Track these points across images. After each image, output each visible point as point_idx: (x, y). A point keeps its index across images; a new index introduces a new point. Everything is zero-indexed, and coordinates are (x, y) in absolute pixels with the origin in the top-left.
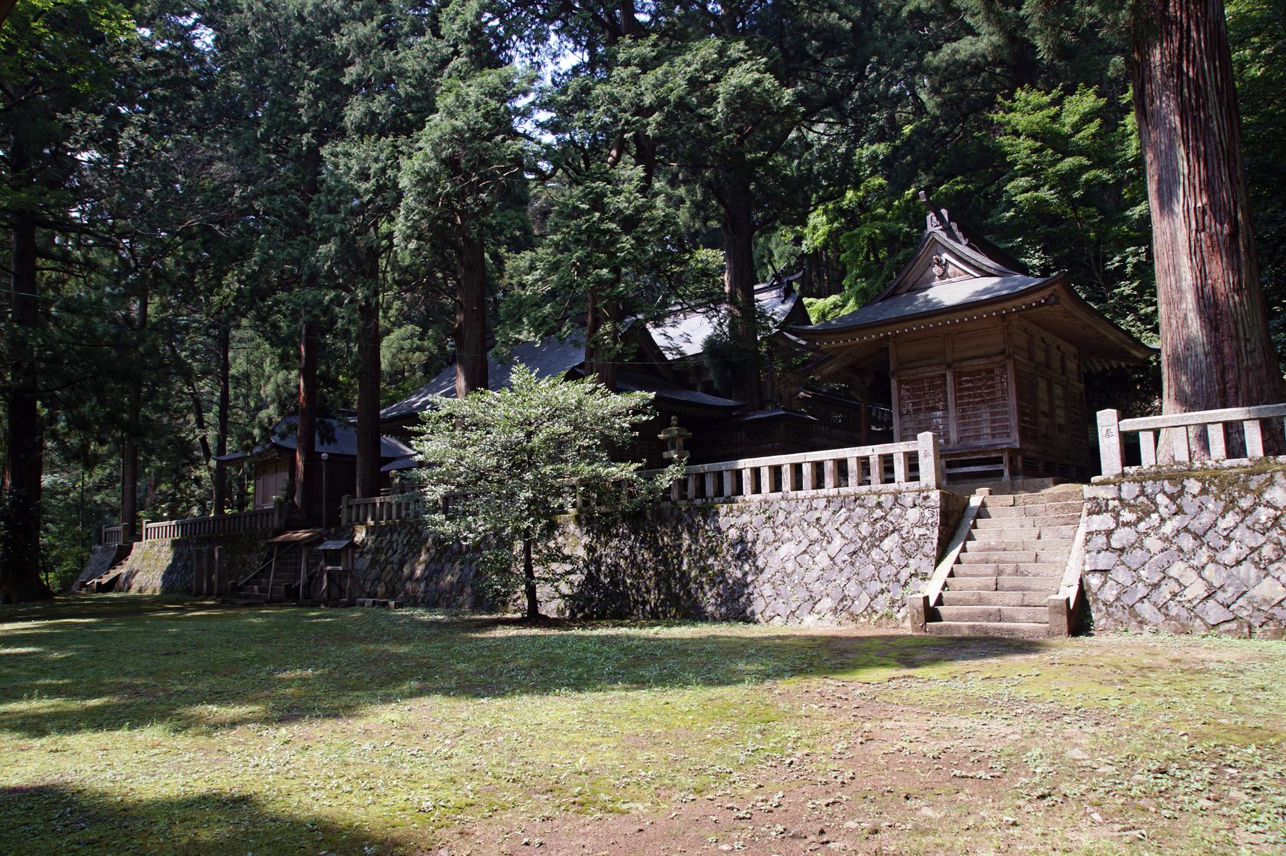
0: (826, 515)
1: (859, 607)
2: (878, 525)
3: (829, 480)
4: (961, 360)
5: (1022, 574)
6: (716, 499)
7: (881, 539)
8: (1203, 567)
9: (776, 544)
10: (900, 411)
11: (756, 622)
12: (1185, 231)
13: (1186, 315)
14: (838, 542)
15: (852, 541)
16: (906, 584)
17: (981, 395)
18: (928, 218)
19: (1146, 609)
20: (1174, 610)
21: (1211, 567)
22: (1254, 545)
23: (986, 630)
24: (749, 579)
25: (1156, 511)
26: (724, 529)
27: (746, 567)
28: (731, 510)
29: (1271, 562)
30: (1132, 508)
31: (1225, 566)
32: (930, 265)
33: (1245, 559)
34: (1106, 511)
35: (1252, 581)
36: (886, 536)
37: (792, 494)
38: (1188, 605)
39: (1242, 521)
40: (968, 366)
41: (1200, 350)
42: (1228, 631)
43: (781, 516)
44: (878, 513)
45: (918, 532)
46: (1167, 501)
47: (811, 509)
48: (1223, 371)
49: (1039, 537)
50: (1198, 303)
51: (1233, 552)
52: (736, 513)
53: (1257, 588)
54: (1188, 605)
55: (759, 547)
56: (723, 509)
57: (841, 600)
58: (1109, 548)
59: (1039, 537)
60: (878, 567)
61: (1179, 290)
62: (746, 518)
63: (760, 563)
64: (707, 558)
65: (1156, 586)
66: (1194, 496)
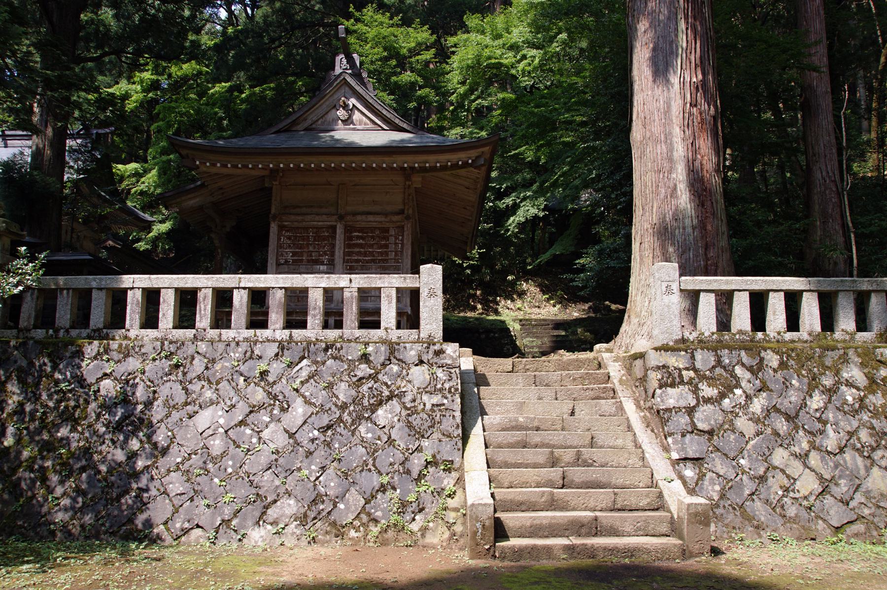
0: (276, 368)
1: (347, 511)
2: (365, 388)
3: (276, 317)
4: (355, 214)
5: (586, 464)
6: (74, 333)
7: (374, 408)
8: (807, 455)
9: (190, 408)
10: (277, 260)
11: (155, 540)
12: (680, 102)
13: (675, 185)
14: (299, 410)
15: (322, 409)
16: (421, 476)
17: (371, 254)
18: (338, 59)
19: (758, 508)
20: (792, 511)
21: (814, 455)
22: (849, 428)
23: (591, 552)
24: (140, 464)
25: (738, 385)
26: (91, 379)
27: (135, 444)
28: (107, 351)
29: (873, 449)
30: (711, 381)
31: (829, 453)
32: (335, 107)
33: (846, 446)
34: (682, 382)
35: (862, 472)
36: (380, 403)
37: (213, 333)
38: (805, 503)
39: (830, 401)
40: (362, 221)
41: (688, 222)
42: (856, 535)
43: (198, 365)
44: (363, 370)
45: (429, 400)
46: (748, 375)
47: (249, 356)
48: (706, 248)
49: (572, 414)
50: (688, 175)
51: (831, 440)
52: (116, 356)
53: (870, 479)
54: (805, 503)
55: (157, 412)
56: (91, 348)
57: (314, 502)
58: (695, 430)
59: (572, 414)
60: (373, 452)
61: (670, 160)
62: (133, 364)
63: (161, 438)
64: (58, 427)
65: (762, 479)
66: (775, 371)
